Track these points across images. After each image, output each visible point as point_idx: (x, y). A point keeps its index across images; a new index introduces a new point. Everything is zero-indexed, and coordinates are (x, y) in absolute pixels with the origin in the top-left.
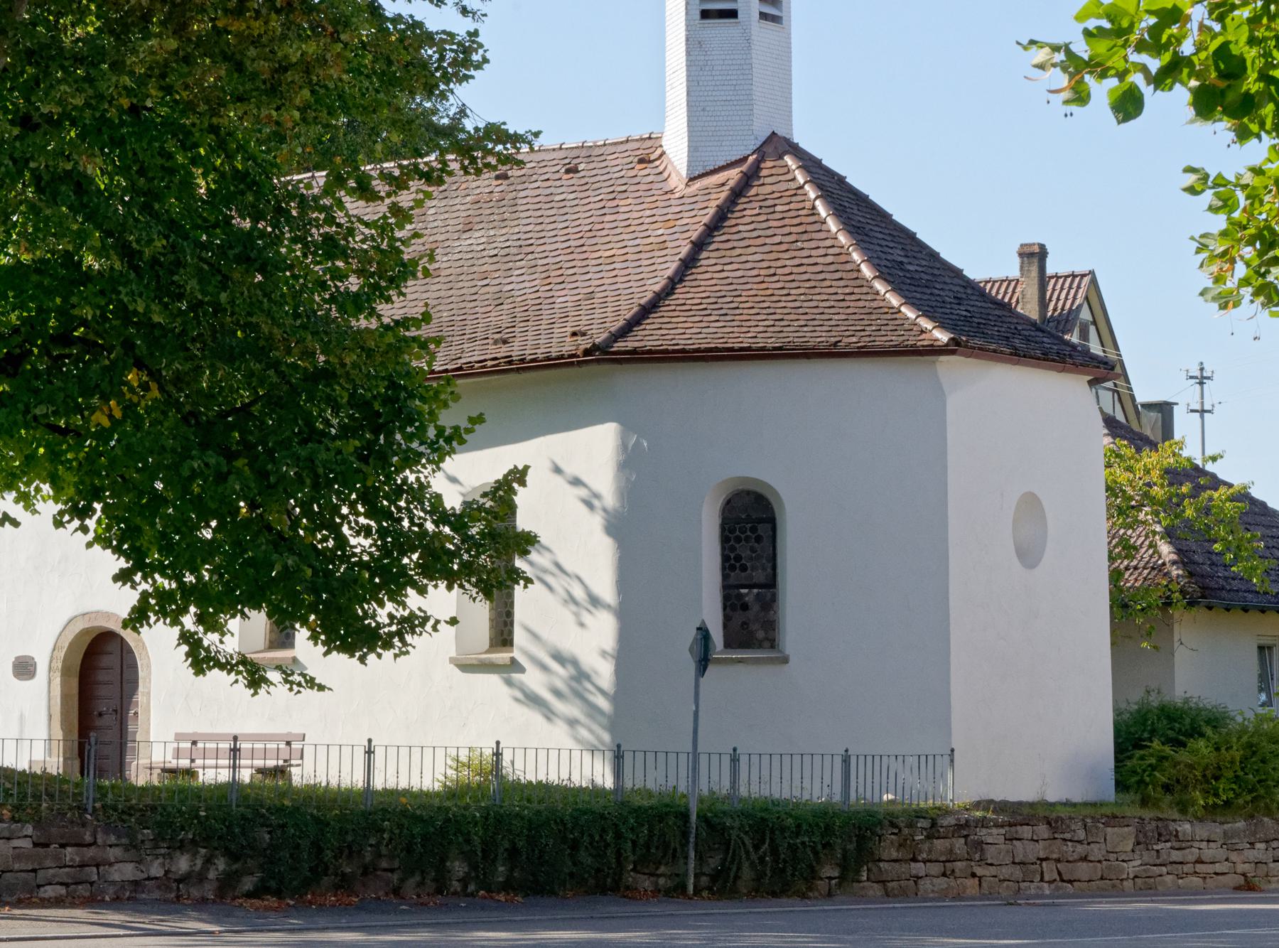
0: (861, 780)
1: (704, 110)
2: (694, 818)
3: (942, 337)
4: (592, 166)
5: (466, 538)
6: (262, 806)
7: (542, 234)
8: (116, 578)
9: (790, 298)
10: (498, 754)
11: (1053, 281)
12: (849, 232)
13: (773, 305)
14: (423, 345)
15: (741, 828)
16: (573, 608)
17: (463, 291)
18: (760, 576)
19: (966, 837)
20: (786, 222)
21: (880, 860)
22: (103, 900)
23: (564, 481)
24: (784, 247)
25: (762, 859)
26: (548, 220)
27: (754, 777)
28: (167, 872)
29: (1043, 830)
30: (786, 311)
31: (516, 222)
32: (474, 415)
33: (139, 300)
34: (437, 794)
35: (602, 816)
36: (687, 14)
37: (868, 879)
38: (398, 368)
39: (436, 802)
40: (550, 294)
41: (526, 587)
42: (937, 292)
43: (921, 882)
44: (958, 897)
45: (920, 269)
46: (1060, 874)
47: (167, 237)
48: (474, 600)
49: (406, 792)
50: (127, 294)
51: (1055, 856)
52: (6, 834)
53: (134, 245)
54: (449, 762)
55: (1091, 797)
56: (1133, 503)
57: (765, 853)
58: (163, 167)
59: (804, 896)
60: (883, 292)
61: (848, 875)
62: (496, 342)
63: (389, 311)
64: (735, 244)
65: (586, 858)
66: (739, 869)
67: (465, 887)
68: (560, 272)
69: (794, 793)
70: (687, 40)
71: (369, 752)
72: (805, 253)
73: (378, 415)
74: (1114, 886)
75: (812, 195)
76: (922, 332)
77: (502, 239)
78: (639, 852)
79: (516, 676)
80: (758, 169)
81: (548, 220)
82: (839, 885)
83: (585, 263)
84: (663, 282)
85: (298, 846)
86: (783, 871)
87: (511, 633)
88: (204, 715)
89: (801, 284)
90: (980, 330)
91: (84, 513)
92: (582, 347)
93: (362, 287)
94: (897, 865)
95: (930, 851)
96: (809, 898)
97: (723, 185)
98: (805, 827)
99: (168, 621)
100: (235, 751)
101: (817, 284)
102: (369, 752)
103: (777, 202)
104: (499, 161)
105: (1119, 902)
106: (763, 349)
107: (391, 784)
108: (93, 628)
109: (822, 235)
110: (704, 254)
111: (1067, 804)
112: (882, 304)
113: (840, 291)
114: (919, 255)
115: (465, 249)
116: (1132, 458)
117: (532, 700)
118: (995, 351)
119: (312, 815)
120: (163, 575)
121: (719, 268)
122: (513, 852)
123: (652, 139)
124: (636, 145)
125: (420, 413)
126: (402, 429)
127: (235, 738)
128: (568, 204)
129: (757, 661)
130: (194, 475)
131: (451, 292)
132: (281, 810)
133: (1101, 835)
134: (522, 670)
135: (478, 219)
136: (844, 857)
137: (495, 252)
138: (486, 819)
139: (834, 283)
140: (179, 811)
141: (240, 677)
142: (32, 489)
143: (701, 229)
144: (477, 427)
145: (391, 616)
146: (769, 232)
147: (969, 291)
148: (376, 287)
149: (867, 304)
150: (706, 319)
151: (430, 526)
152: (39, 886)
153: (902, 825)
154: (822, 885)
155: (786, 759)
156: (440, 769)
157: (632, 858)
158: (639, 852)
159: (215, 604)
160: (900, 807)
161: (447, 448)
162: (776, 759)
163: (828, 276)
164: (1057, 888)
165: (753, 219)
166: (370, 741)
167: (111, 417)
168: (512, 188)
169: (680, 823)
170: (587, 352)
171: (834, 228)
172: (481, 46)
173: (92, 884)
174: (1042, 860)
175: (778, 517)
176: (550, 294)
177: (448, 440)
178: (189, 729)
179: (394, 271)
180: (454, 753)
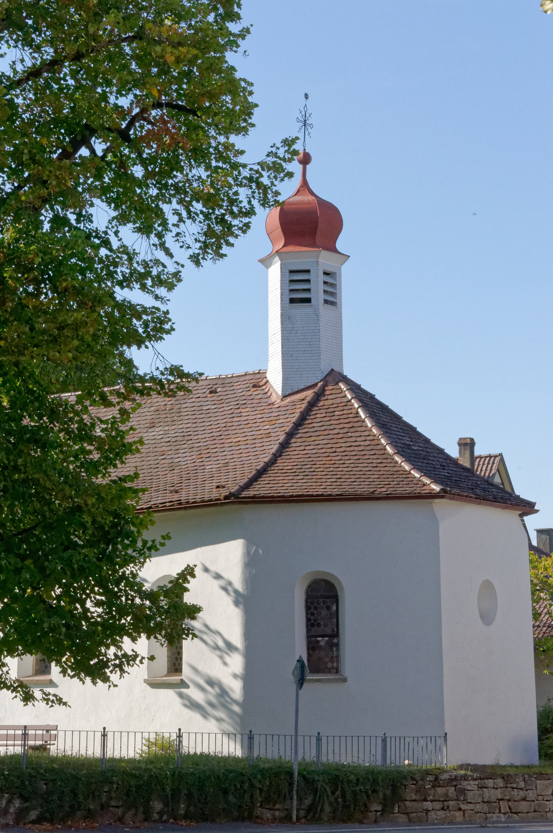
1: (291, 356)
2: (296, 774)
3: (436, 488)
4: (225, 389)
7: (196, 429)
9: (345, 466)
10: (180, 736)
11: (478, 460)
12: (380, 427)
14: (136, 491)
15: (324, 781)
16: (218, 653)
19: (455, 786)
20: (342, 421)
21: (406, 800)
23: (213, 572)
24: (340, 436)
25: (336, 799)
29: (500, 782)
31: (181, 422)
32: (164, 534)
35: (242, 774)
36: (281, 300)
37: (399, 812)
38: (121, 506)
40: (202, 464)
41: (192, 639)
43: (430, 813)
44: (451, 823)
46: (510, 808)
49: (121, 760)
51: (507, 798)
54: (144, 742)
55: (525, 763)
56: (538, 588)
57: (338, 796)
59: (361, 822)
60: (400, 462)
61: (387, 808)
62: (171, 492)
63: (115, 473)
64: (312, 434)
66: (322, 806)
68: (208, 451)
69: (354, 760)
71: (104, 735)
72: (353, 439)
74: (542, 816)
75: (356, 406)
76: (424, 485)
78: (263, 795)
79: (184, 690)
80: (323, 391)
82: (382, 815)
83: (222, 446)
86: (348, 807)
87: (180, 665)
89: (351, 457)
90: (457, 484)
92: (223, 495)
93: (100, 458)
94: (416, 803)
96: (363, 823)
97: (303, 400)
98: (361, 780)
101: (361, 457)
102: (104, 735)
103: (335, 409)
105: (546, 826)
106: (330, 495)
107: (117, 755)
109: (363, 429)
110: (293, 440)
111: (511, 766)
112: (399, 469)
113: (374, 461)
114: (418, 441)
115: (151, 438)
116: (537, 561)
117: (193, 705)
118: (467, 496)
119: (71, 774)
121: (302, 448)
123: (261, 374)
124: (251, 377)
125: (133, 532)
127: (25, 727)
129: (328, 681)
131: (143, 463)
132: (53, 770)
133: (534, 785)
135: (158, 421)
136: (385, 799)
137: (169, 439)
138: (173, 775)
139: (371, 457)
143: (291, 425)
145: (115, 655)
146: (332, 427)
147: (448, 462)
148: (107, 458)
150: (296, 478)
153: (418, 779)
155: (361, 739)
156: (139, 746)
157: (260, 799)
158: (263, 795)
160: (415, 768)
163: (367, 453)
164: (509, 817)
165: (322, 419)
166: (104, 728)
168: (178, 402)
170: (226, 498)
171: (369, 425)
174: (500, 800)
175: (339, 594)
176: (202, 464)
180: (147, 737)
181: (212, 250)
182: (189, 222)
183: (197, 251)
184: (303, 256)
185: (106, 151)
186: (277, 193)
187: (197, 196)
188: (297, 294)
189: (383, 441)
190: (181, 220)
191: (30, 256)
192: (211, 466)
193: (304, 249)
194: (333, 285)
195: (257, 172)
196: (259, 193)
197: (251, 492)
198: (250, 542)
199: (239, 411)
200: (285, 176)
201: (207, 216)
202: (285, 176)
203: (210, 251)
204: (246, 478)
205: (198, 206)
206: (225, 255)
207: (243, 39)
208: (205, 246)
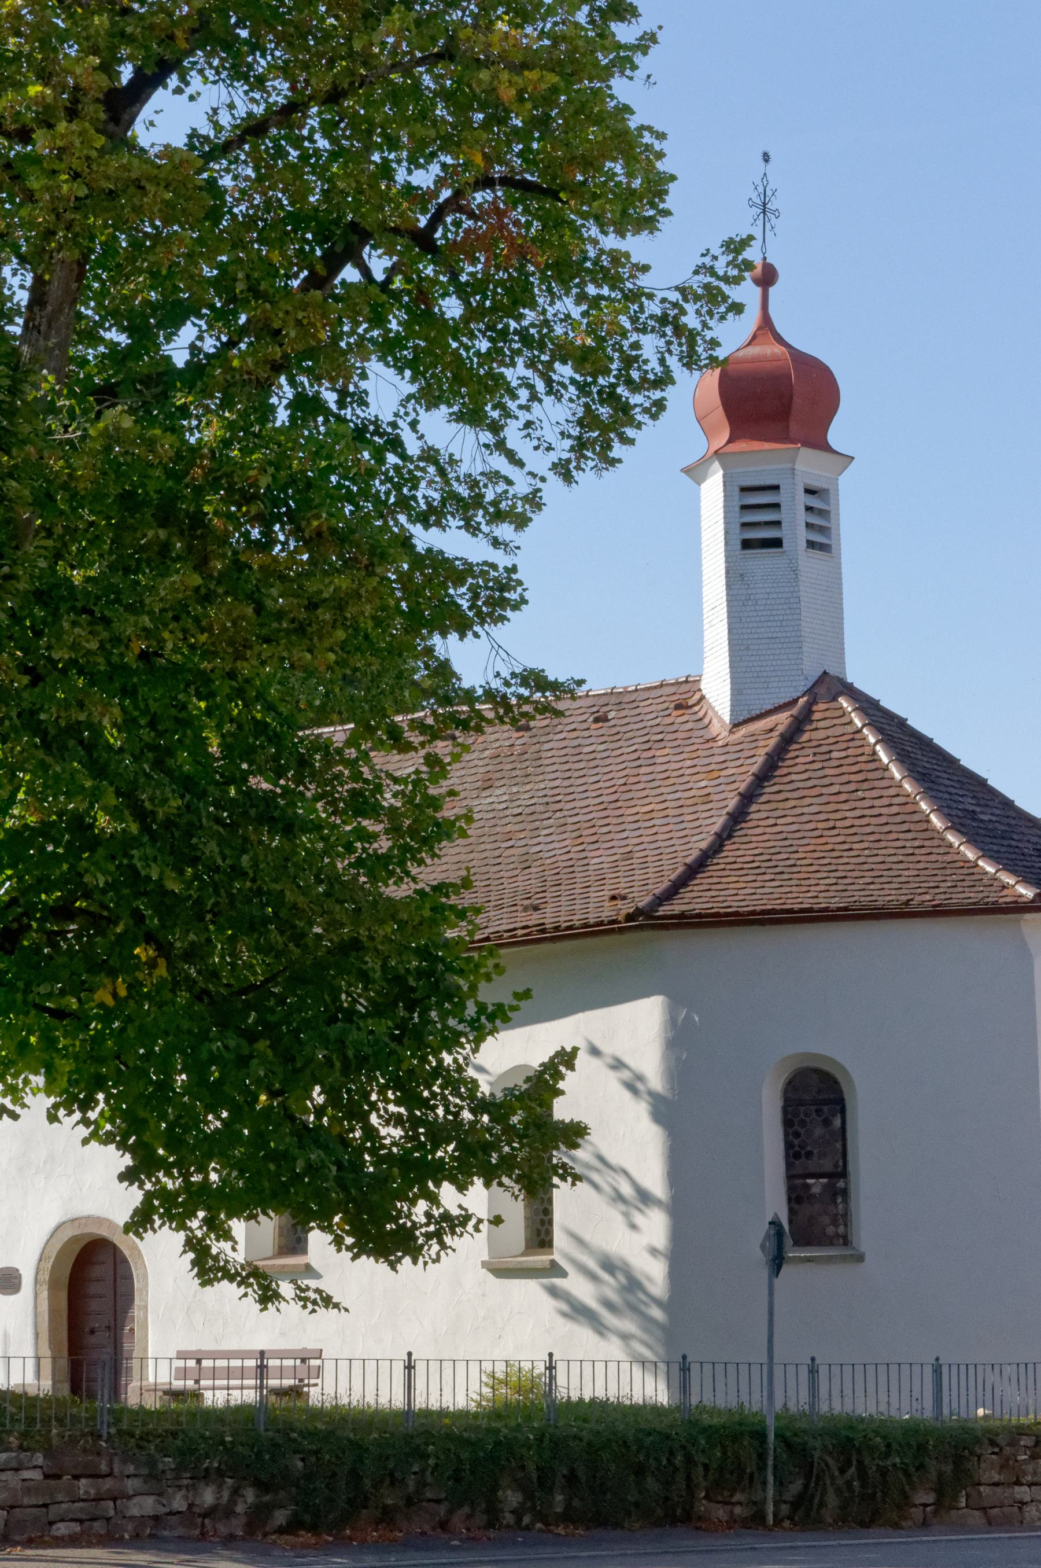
0: (955, 1393)
1: (748, 649)
2: (771, 1437)
3: (1027, 892)
4: (623, 713)
5: (509, 1129)
6: (293, 1430)
7: (571, 790)
8: (122, 1177)
9: (852, 853)
10: (551, 1367)
13: (833, 861)
14: (462, 914)
16: (622, 1207)
17: (484, 855)
18: (828, 1165)
20: (844, 769)
21: (980, 1484)
22: (122, 1538)
23: (607, 1059)
25: (849, 1484)
26: (576, 774)
27: (836, 1393)
28: (191, 1506)
30: (849, 867)
31: (541, 777)
32: (520, 990)
33: (153, 864)
34: (463, 1415)
36: (726, 544)
37: (967, 1506)
39: (484, 1423)
42: (1013, 843)
43: (1026, 1508)
45: (994, 819)
47: (182, 797)
48: (516, 1198)
49: (443, 1413)
50: (140, 859)
52: (14, 1465)
53: (147, 804)
54: (484, 1379)
58: (176, 719)
59: (896, 1526)
61: (944, 1501)
62: (526, 909)
63: (429, 873)
65: (651, 1484)
66: (823, 1495)
67: (519, 1520)
68: (593, 830)
69: (881, 1409)
70: (727, 572)
71: (410, 1367)
72: (867, 803)
73: (413, 990)
75: (872, 740)
76: (1004, 887)
77: (526, 796)
79: (558, 1281)
80: (805, 709)
81: (576, 774)
82: (936, 1513)
83: (620, 820)
84: (710, 839)
85: (334, 1475)
87: (549, 1232)
88: (195, 1330)
89: (865, 838)
91: (87, 1105)
92: (624, 912)
93: (391, 849)
94: (999, 1490)
95: (1035, 1474)
96: (902, 1528)
97: (771, 730)
98: (895, 1446)
99: (174, 1225)
100: (262, 1370)
101: (882, 837)
102: (410, 1367)
103: (832, 747)
104: (536, 709)
106: (826, 909)
107: (434, 1405)
108: (91, 1234)
110: (754, 807)
112: (956, 858)
115: (485, 808)
120: (169, 1174)
121: (771, 822)
122: (572, 1479)
123: (691, 684)
124: (672, 690)
126: (439, 1005)
127: (262, 1353)
128: (599, 756)
129: (829, 1259)
130: (213, 1059)
131: (471, 856)
134: (564, 1274)
135: (499, 775)
137: (519, 811)
138: (542, 1441)
139: (901, 836)
140: (202, 1437)
141: (250, 1290)
142: (20, 1081)
143: (749, 779)
144: (522, 1004)
146: (826, 781)
149: (940, 858)
150: (760, 878)
151: (467, 1115)
152: (51, 1523)
153: (1003, 1443)
154: (917, 1513)
155: (871, 1370)
156: (475, 1386)
157: (704, 1484)
159: (220, 1206)
160: (998, 1423)
161: (489, 1026)
162: (859, 1369)
166: (410, 1354)
167: (115, 995)
168: (535, 740)
169: (756, 1443)
170: (629, 917)
171: (898, 776)
172: (520, 583)
173: (108, 1519)
175: (846, 1097)
177: (491, 1018)
178: (192, 1345)
179: (426, 831)
180: (490, 1369)
181: (594, 452)
182: (548, 400)
183: (565, 455)
184: (766, 460)
185: (391, 272)
186: (714, 343)
187: (563, 352)
188: (756, 530)
189: (923, 806)
190: (534, 397)
191: (252, 473)
192: (599, 859)
193: (767, 446)
194: (823, 513)
195: (675, 305)
196: (680, 345)
197: (675, 907)
198: (675, 1001)
199: (650, 754)
200: (729, 309)
201: (583, 389)
202: (729, 309)
203: (589, 454)
204: (665, 879)
205: (564, 371)
206: (619, 461)
207: (645, 54)
208: (580, 446)
